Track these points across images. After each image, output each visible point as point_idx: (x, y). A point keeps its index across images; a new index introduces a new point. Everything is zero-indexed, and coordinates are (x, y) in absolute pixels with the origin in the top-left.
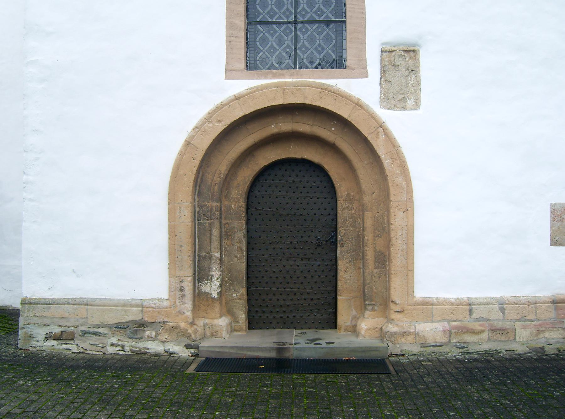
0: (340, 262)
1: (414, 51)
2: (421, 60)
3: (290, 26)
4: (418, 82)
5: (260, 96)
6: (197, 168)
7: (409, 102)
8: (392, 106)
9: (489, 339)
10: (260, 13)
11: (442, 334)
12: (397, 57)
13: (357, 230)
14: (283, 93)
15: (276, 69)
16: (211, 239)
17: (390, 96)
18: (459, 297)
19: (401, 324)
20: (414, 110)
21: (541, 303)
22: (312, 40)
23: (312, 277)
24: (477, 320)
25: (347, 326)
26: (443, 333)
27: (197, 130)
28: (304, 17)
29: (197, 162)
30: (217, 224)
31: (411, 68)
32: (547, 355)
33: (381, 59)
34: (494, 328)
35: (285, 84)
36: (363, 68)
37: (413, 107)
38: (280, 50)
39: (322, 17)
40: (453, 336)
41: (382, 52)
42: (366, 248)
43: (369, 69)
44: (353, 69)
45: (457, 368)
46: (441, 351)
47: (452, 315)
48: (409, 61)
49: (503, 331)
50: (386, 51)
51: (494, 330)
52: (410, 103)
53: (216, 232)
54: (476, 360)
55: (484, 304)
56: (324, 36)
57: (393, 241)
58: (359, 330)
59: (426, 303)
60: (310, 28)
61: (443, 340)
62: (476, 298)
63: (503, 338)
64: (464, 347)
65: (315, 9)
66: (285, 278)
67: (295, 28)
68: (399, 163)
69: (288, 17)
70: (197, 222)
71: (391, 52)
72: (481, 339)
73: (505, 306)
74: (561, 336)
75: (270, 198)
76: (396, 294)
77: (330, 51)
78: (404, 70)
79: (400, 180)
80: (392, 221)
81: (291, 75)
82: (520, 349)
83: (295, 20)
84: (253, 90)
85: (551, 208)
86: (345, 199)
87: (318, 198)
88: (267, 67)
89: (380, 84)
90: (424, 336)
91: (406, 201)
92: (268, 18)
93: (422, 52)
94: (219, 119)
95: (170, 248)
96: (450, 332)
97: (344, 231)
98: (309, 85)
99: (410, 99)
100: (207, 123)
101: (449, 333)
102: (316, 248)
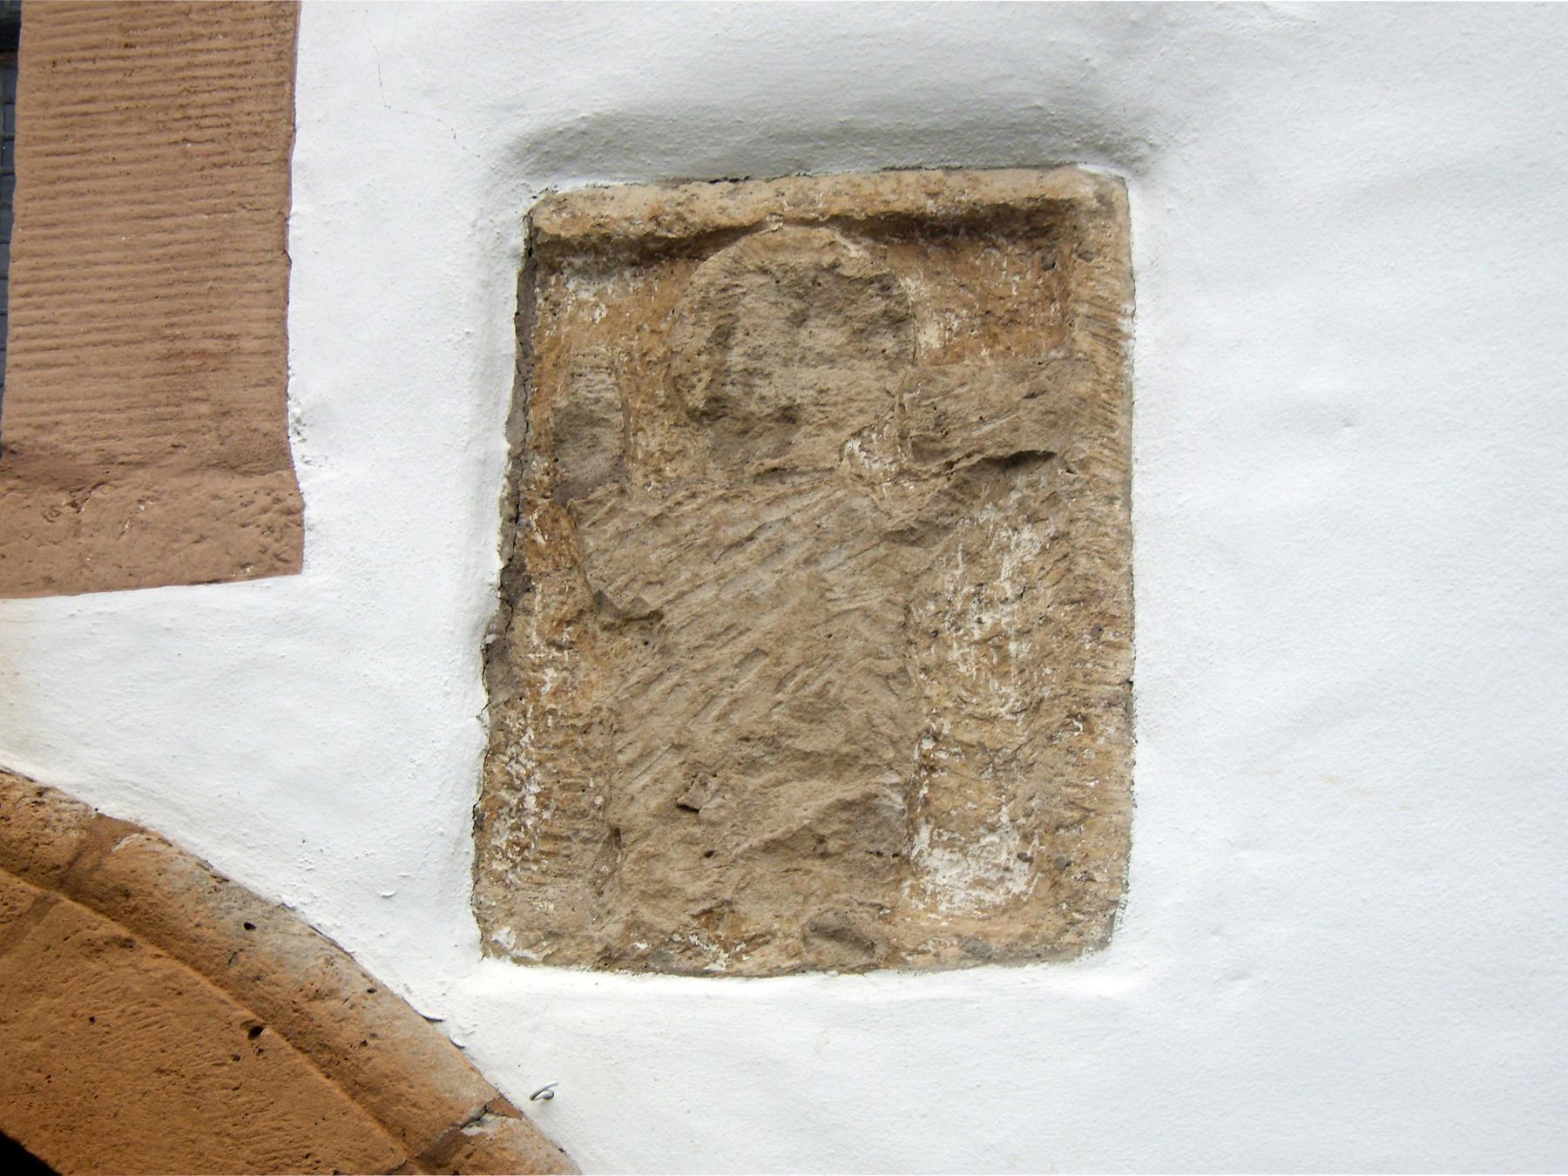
1: (1040, 226)
4: (1097, 609)
8: (665, 918)
12: (760, 309)
17: (642, 796)
31: (994, 436)
36: (228, 465)
43: (324, 477)
50: (602, 251)
52: (951, 881)
71: (663, 250)
99: (961, 834)
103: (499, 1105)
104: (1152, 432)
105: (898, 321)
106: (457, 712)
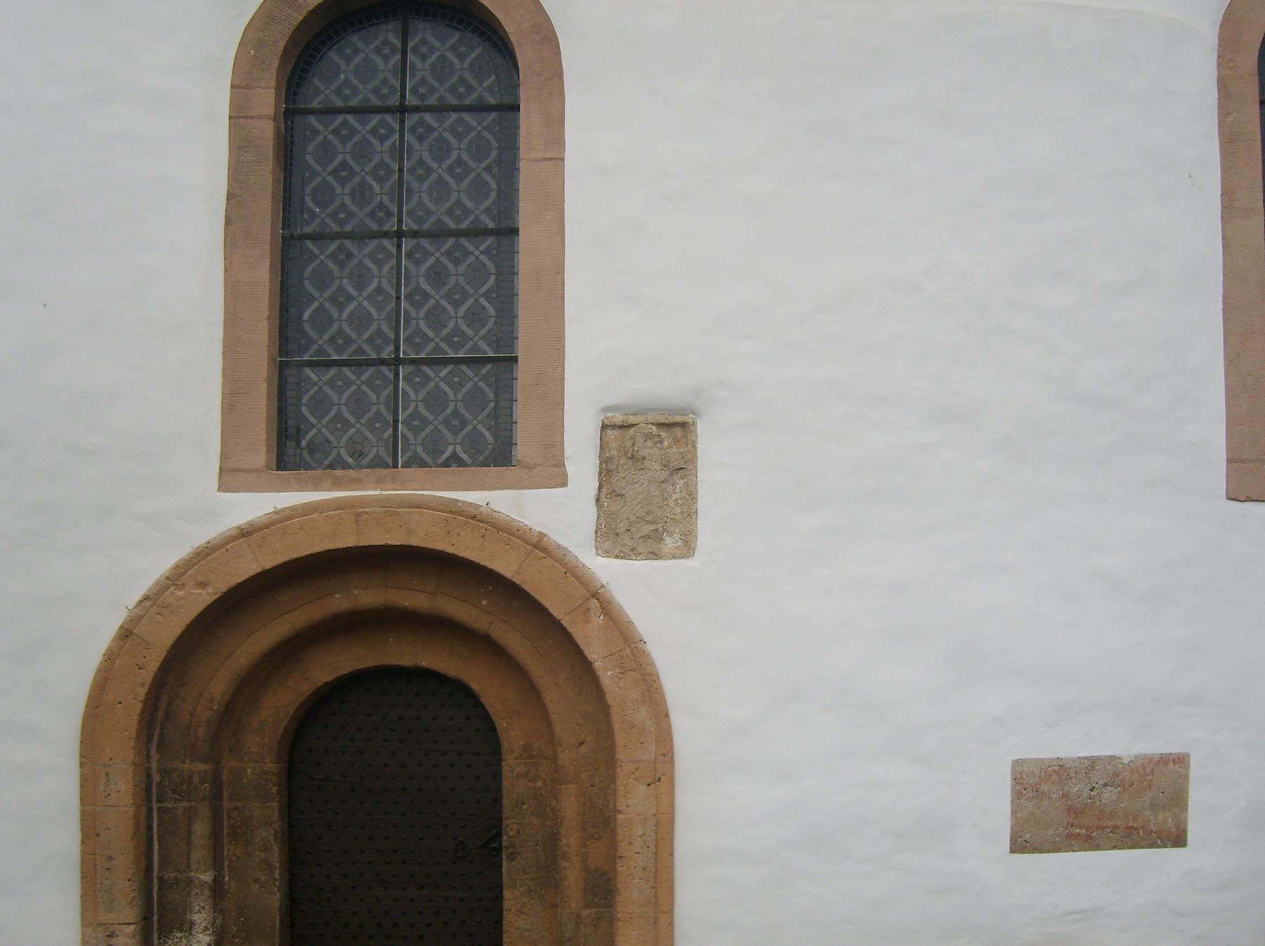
0: (507, 894)
1: (683, 425)
2: (700, 446)
3: (384, 369)
4: (692, 496)
5: (301, 528)
6: (147, 687)
7: (669, 541)
8: (626, 550)
10: (311, 342)
12: (639, 439)
13: (548, 823)
14: (357, 521)
15: (346, 466)
16: (189, 844)
17: (622, 528)
22: (436, 401)
23: (446, 924)
27: (149, 603)
28: (418, 348)
29: (148, 675)
30: (204, 810)
31: (675, 464)
33: (601, 446)
35: (362, 502)
36: (555, 466)
37: (678, 552)
38: (358, 425)
39: (464, 350)
42: (564, 864)
43: (571, 468)
44: (530, 467)
48: (670, 447)
50: (614, 426)
52: (670, 543)
53: (201, 828)
56: (467, 393)
57: (623, 848)
60: (432, 374)
65: (445, 332)
66: (379, 925)
67: (397, 375)
69: (379, 349)
70: (155, 806)
71: (624, 427)
75: (344, 753)
78: (658, 468)
79: (642, 714)
81: (379, 483)
83: (397, 357)
84: (283, 514)
85: (1013, 771)
86: (521, 757)
87: (461, 754)
88: (326, 462)
89: (597, 500)
91: (655, 761)
92: (331, 352)
93: (702, 428)
94: (200, 579)
95: (83, 862)
97: (517, 824)
98: (420, 505)
99: (671, 534)
100: (172, 589)
102: (454, 863)
103: (603, 586)
104: (700, 464)
105: (661, 442)
106: (592, 511)
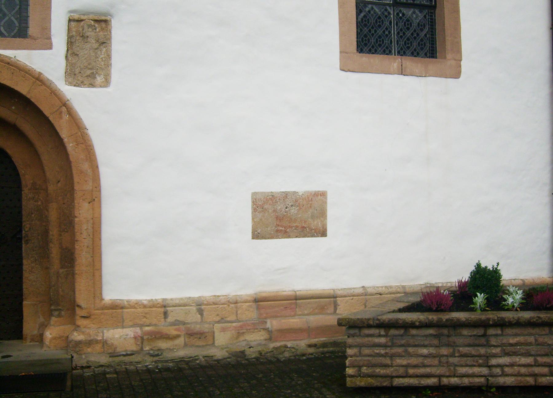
0: (25, 262)
1: (106, 21)
4: (109, 57)
8: (79, 82)
9: (186, 345)
11: (133, 341)
12: (86, 27)
18: (154, 298)
19: (88, 331)
20: (77, 86)
21: (243, 302)
24: (173, 324)
25: (34, 335)
26: (134, 340)
32: (247, 360)
34: (190, 332)
37: (103, 84)
40: (145, 343)
41: (70, 20)
43: (54, 40)
44: (35, 39)
45: (141, 380)
46: (132, 360)
47: (145, 319)
48: (99, 32)
49: (200, 335)
50: (74, 20)
51: (191, 334)
52: (99, 79)
54: (168, 369)
55: (180, 306)
58: (47, 340)
59: (116, 306)
61: (134, 348)
62: (172, 299)
63: (201, 343)
64: (158, 355)
68: (85, 147)
71: (79, 21)
72: (176, 345)
73: (203, 307)
74: (262, 338)
76: (81, 298)
77: (12, 18)
78: (94, 42)
79: (86, 166)
80: (76, 213)
82: (218, 354)
89: (66, 57)
90: (112, 344)
91: (92, 191)
96: (142, 338)
99: (99, 75)
101: (141, 340)
